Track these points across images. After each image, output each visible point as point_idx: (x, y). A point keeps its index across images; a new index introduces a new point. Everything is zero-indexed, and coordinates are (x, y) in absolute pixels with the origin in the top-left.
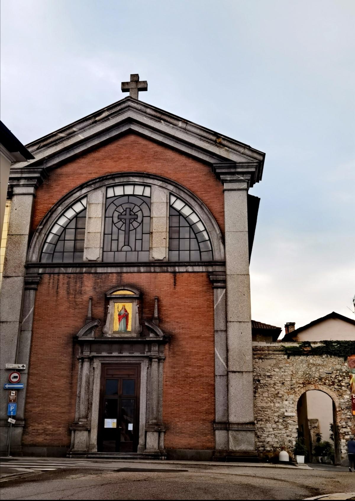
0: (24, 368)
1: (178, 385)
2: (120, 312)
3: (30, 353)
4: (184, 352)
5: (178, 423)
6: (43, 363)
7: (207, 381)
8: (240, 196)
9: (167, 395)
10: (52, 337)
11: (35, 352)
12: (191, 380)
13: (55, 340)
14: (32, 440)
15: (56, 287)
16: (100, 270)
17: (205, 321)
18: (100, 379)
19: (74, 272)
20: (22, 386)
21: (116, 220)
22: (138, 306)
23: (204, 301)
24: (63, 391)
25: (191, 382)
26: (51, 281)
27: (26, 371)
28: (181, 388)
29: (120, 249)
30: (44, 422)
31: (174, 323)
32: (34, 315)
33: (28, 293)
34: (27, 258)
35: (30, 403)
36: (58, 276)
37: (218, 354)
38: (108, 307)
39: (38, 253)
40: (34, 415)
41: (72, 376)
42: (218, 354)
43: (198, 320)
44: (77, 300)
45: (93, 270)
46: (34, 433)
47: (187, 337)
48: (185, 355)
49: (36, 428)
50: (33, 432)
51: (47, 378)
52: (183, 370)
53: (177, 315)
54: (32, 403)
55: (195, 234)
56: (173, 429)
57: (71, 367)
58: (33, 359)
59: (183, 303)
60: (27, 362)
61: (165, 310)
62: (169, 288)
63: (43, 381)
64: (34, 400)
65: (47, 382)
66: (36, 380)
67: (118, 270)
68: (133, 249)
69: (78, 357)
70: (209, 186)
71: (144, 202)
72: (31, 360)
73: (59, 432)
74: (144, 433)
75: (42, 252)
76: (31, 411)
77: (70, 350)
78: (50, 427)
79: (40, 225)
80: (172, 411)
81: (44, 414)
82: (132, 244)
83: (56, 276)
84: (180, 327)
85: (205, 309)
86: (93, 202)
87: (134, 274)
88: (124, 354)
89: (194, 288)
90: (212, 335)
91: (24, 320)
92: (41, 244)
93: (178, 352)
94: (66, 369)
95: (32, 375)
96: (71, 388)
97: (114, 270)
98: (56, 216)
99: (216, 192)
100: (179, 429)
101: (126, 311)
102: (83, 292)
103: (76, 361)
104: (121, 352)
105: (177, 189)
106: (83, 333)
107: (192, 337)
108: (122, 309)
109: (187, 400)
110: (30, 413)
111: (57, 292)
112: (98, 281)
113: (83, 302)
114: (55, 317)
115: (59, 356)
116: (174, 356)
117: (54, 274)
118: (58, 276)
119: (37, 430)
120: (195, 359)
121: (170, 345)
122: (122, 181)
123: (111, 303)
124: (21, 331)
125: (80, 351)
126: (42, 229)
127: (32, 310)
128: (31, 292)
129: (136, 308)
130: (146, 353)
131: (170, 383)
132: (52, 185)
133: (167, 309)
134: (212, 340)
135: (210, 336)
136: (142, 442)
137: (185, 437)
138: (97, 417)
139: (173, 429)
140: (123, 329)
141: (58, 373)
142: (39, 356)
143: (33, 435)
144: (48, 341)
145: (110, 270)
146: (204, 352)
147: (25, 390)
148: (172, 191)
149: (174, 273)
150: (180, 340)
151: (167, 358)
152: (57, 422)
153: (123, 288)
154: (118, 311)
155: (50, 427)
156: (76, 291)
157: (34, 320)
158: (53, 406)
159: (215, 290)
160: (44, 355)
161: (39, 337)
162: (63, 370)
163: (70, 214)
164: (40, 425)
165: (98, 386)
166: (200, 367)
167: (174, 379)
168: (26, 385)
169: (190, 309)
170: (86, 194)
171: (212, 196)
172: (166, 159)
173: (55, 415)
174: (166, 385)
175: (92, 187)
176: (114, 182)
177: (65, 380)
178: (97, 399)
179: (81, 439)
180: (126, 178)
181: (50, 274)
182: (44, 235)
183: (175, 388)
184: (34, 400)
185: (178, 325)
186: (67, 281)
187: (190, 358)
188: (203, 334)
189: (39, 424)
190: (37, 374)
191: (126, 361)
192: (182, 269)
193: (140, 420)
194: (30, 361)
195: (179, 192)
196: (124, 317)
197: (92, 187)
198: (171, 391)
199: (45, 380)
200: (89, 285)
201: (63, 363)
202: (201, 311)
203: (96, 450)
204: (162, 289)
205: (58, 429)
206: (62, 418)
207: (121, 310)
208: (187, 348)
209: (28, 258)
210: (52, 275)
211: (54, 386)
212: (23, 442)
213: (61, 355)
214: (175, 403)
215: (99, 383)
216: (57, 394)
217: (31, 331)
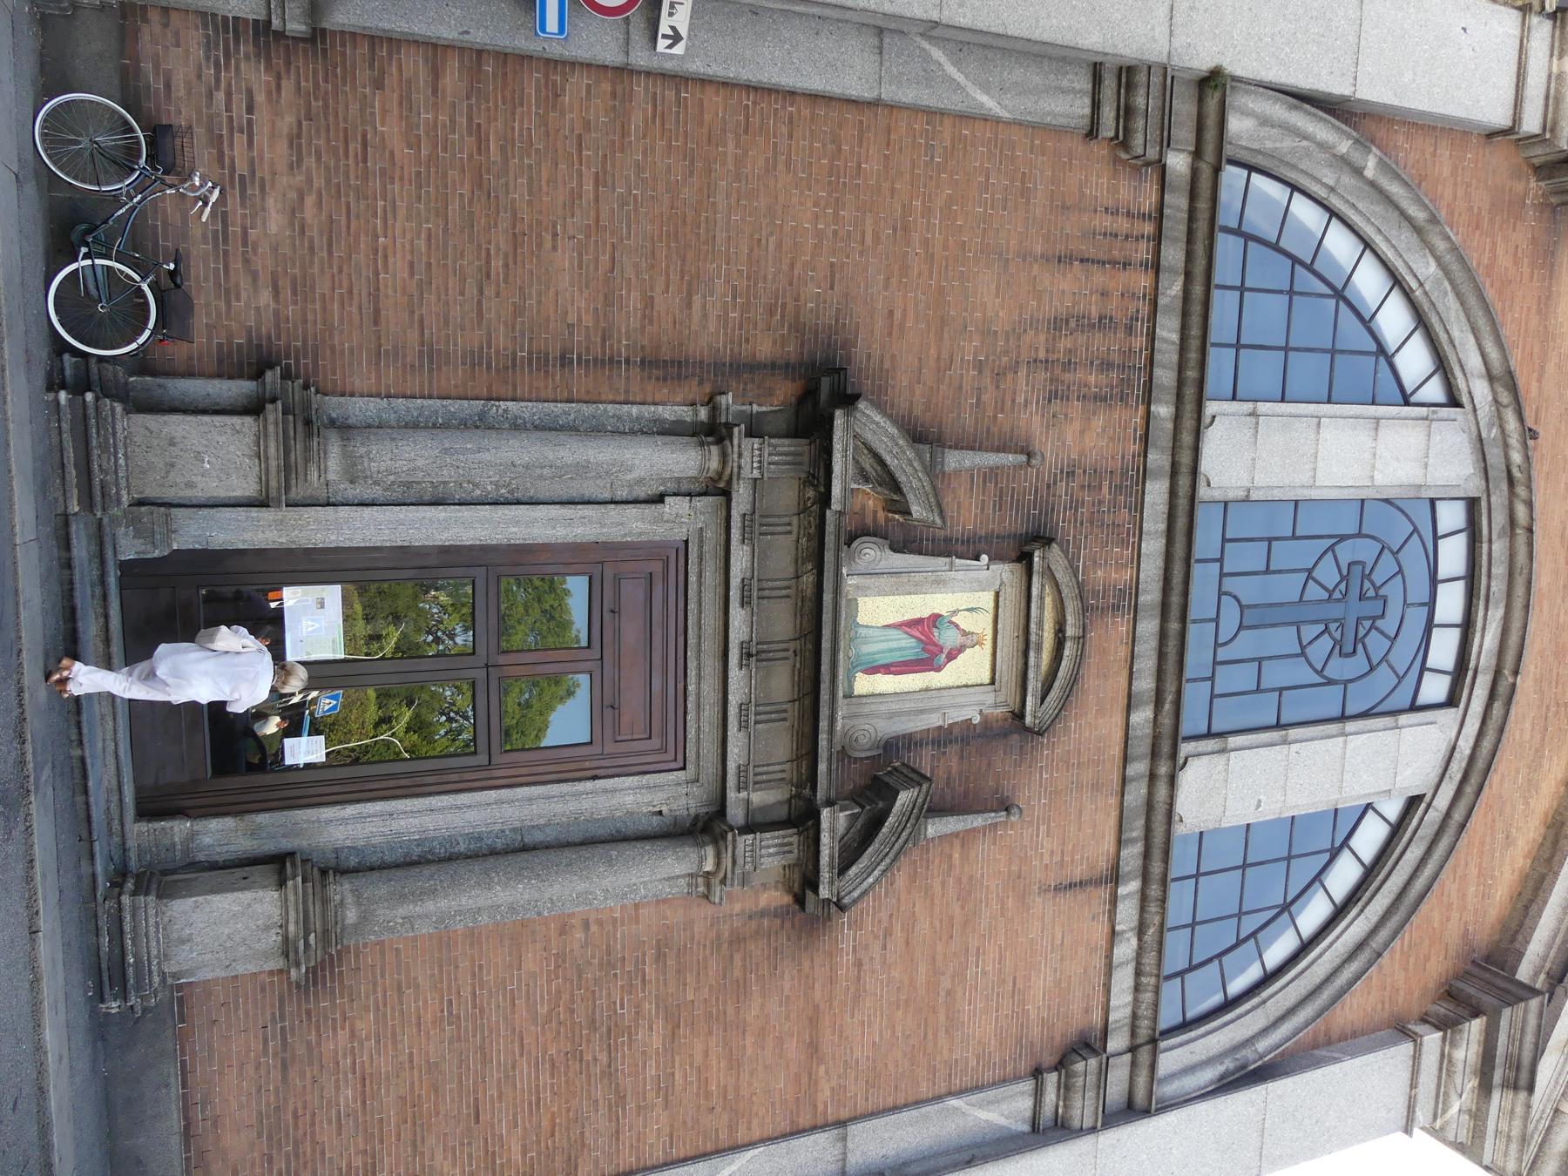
0: (662, 44)
1: (566, 997)
2: (951, 622)
3: (749, 88)
4: (741, 990)
5: (343, 1035)
6: (692, 173)
7: (589, 1140)
8: (1389, 1111)
9: (507, 942)
10: (835, 233)
11: (756, 121)
12: (595, 1060)
13: (817, 247)
14: (168, 86)
15: (1091, 252)
16: (1156, 493)
17: (891, 1068)
18: (592, 538)
19: (1157, 357)
20: (552, 24)
21: (1346, 553)
22: (977, 720)
23: (979, 1042)
24: (518, 311)
25: (588, 1057)
26: (1123, 224)
27: (640, 59)
28: (550, 1011)
29: (1229, 583)
30: (309, 180)
31: (884, 915)
32: (963, 117)
33: (1077, 86)
34: (1248, 82)
35: (436, 74)
36: (1145, 265)
37: (734, 1168)
38: (977, 558)
39: (1256, 146)
40: (354, 108)
41: (613, 362)
42: (734, 1168)
43: (894, 1032)
44: (1023, 372)
45: (1158, 459)
46: (228, 109)
47: (818, 993)
48: (725, 1002)
49: (262, 116)
50: (229, 94)
51: (597, 200)
52: (649, 1007)
53: (924, 926)
54: (435, 92)
55: (1254, 934)
56: (308, 1013)
57: (666, 354)
58: (715, 101)
59: (974, 943)
60: (697, 67)
61: (950, 857)
62: (1046, 860)
63: (580, 175)
64: (453, 105)
65: (575, 195)
66: (587, 125)
67: (1150, 595)
68: (1223, 654)
69: (726, 400)
70: (1427, 958)
71: (1400, 679)
72: (710, 90)
73: (244, 283)
74: (270, 847)
75: (1251, 168)
76: (379, 84)
77: (764, 348)
78: (275, 222)
79: (1383, 165)
80: (417, 986)
81: (366, 175)
82: (1248, 644)
83: (1143, 252)
84: (867, 947)
85: (946, 1053)
86: (1436, 438)
87: (1125, 673)
88: (735, 673)
89: (1040, 985)
90: (825, 1112)
91: (937, 54)
92: (1294, 167)
93: (744, 959)
94: (651, 322)
95: (614, 95)
96: (540, 362)
97: (1152, 568)
98: (1401, 247)
99: (1402, 993)
100: (309, 1043)
101: (951, 657)
102: (1056, 406)
103: (701, 383)
104: (749, 655)
105: (1436, 827)
106: (869, 436)
107: (814, 1021)
108: (965, 633)
109: (485, 1060)
110: (364, 75)
111: (1065, 260)
112: (1105, 490)
113: (1013, 409)
114: (945, 248)
115: (728, 275)
116: (719, 946)
117: (1158, 237)
118: (1145, 265)
119: (250, 122)
120: (706, 1053)
121: (776, 916)
122: (1494, 570)
123: (1006, 573)
124: (880, 31)
125: (755, 408)
126: (1358, 172)
127: (988, 102)
128: (1078, 102)
129: (970, 711)
130: (743, 794)
131: (576, 946)
132: (1519, 224)
133: (951, 867)
134: (801, 1120)
135: (821, 1107)
136: (207, 840)
137: (259, 1090)
138: (357, 542)
139: (308, 1013)
140: (865, 649)
141: (630, 272)
142: (731, 145)
143: (210, 96)
144: (816, 204)
145: (1153, 547)
146: (745, 1092)
147: (522, 43)
148: (1429, 806)
149: (1114, 877)
150: (800, 964)
151: (709, 910)
152: (316, 270)
153: (1070, 631)
154: (955, 613)
155: (275, 222)
156: (1068, 366)
157: (931, 113)
158: (422, 244)
159: (1028, 1086)
160: (738, 178)
161: (839, 149)
162: (649, 303)
163: (1394, 320)
164: (282, 147)
165: (550, 532)
166: (665, 1089)
167: (601, 965)
168: (556, 51)
169: (946, 983)
170: (1465, 399)
171: (1389, 980)
172: (1542, 757)
173: (361, 257)
174: (563, 930)
175: (1490, 426)
176: (1494, 537)
177: (588, 320)
178: (471, 534)
179: (199, 457)
180: (1504, 587)
181: (1159, 216)
182: (1331, 183)
183: (549, 981)
184: (453, 105)
185: (876, 937)
186: (1118, 316)
187: (710, 1033)
188: (827, 1072)
189: (295, 140)
190: (624, 134)
191: (702, 686)
192: (1127, 914)
193: (350, 810)
194: (704, 81)
195: (1422, 838)
196: (924, 649)
197: (1489, 431)
198: (530, 963)
199: (589, 187)
200: (1090, 441)
201: (689, 305)
202: (935, 1035)
203: (128, 554)
204: (1043, 828)
205: (264, 278)
206: (342, 304)
207: (957, 626)
208: (763, 1006)
209: (1247, 92)
210: (1148, 228)
211: (548, 244)
212: (154, 16)
213: (735, 288)
214: (466, 992)
215: (570, 539)
216: (497, 264)
217: (875, 94)
